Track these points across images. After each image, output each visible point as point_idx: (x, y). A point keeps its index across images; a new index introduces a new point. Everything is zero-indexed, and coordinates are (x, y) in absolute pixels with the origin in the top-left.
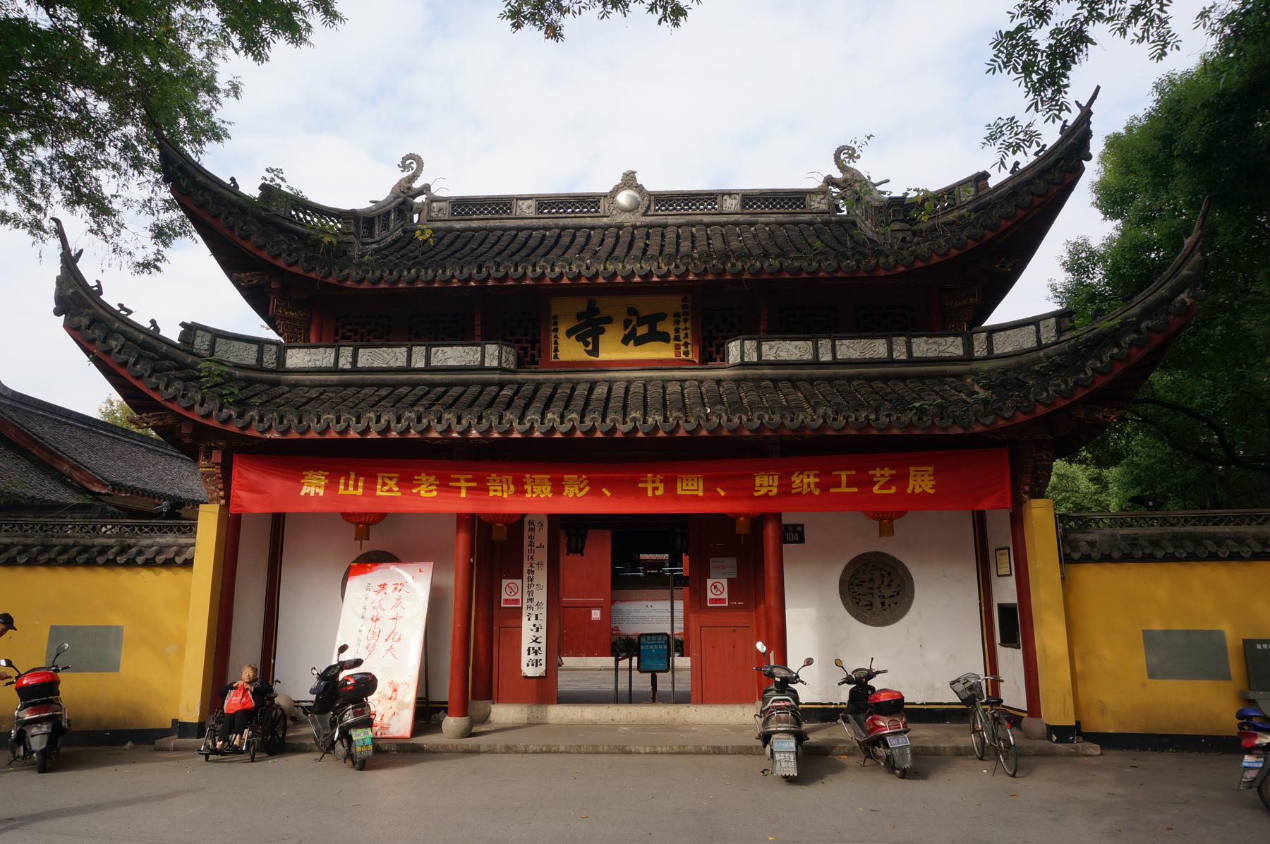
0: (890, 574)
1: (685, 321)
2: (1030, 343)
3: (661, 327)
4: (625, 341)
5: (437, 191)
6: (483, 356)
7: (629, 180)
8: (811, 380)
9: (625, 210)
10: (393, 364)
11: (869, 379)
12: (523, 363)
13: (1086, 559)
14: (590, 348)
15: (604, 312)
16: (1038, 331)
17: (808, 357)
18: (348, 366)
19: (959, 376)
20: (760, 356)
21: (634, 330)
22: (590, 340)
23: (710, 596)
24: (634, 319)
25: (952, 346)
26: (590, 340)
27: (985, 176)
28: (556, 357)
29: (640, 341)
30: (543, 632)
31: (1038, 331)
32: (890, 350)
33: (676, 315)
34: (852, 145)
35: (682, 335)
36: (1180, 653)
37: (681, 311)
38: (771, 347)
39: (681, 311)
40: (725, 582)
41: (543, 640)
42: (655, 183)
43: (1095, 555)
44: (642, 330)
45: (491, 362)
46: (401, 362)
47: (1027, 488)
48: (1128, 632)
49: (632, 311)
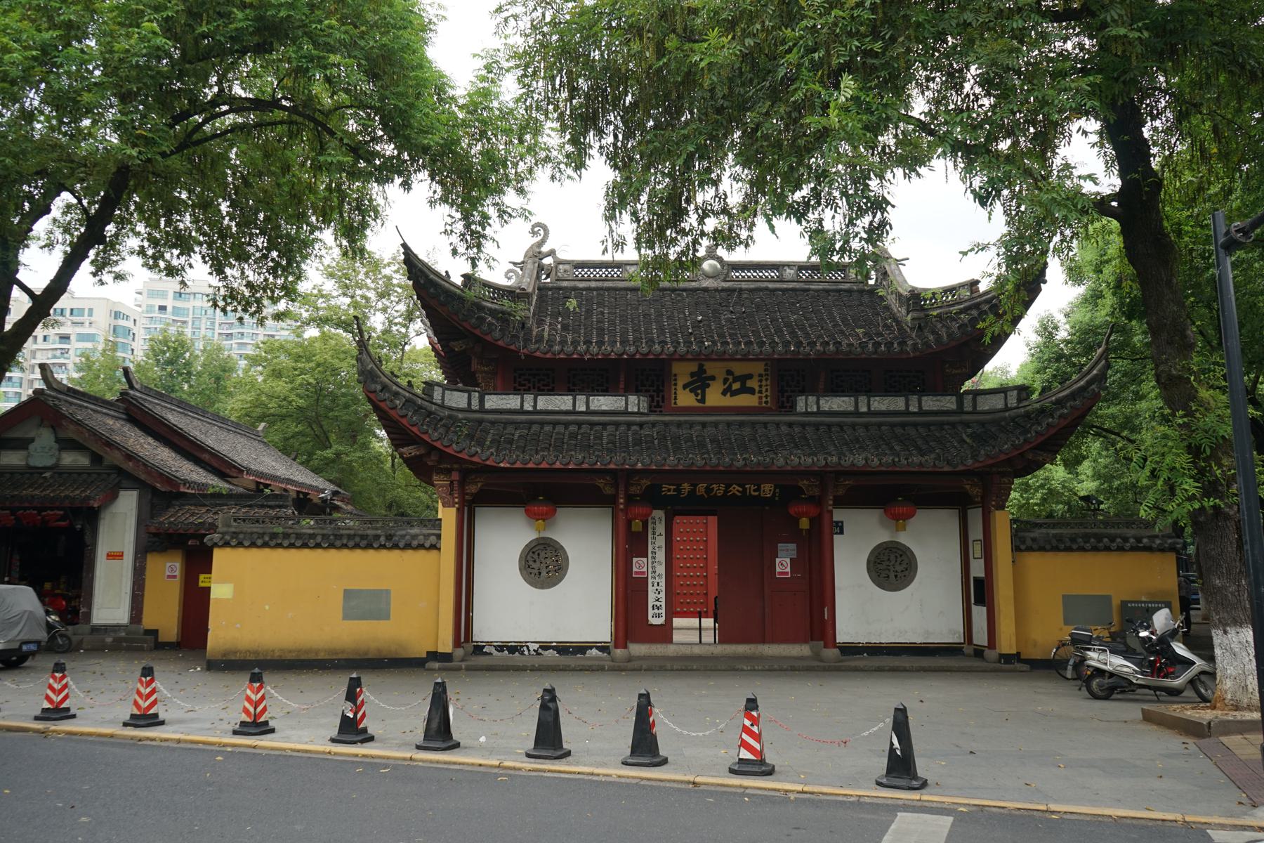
2: (1001, 405)
3: (749, 384)
4: (724, 393)
5: (562, 256)
6: (627, 404)
8: (853, 426)
9: (708, 276)
10: (563, 408)
11: (892, 425)
13: (1030, 549)
15: (710, 372)
16: (1006, 398)
17: (851, 409)
18: (531, 409)
19: (953, 425)
21: (730, 386)
23: (778, 570)
24: (731, 378)
25: (949, 403)
27: (977, 282)
30: (663, 595)
31: (1006, 398)
32: (907, 405)
40: (788, 560)
41: (663, 600)
43: (1035, 546)
44: (736, 386)
45: (633, 408)
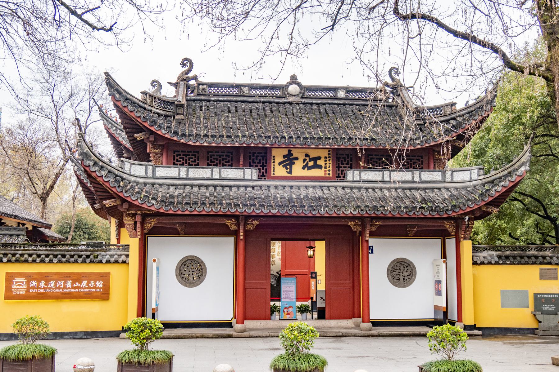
0: (407, 266)
1: (329, 160)
3: (319, 162)
4: (303, 168)
7: (294, 80)
12: (261, 176)
14: (288, 170)
15: (295, 155)
16: (471, 174)
20: (360, 177)
21: (307, 163)
22: (288, 167)
24: (308, 159)
25: (437, 176)
26: (288, 167)
28: (274, 174)
29: (310, 168)
31: (471, 174)
32: (413, 177)
33: (326, 157)
34: (396, 66)
35: (328, 166)
36: (510, 298)
37: (328, 156)
38: (366, 174)
39: (328, 156)
42: (306, 82)
43: (486, 262)
45: (248, 177)
46: (208, 175)
47: (463, 236)
48: (502, 290)
49: (307, 155)
